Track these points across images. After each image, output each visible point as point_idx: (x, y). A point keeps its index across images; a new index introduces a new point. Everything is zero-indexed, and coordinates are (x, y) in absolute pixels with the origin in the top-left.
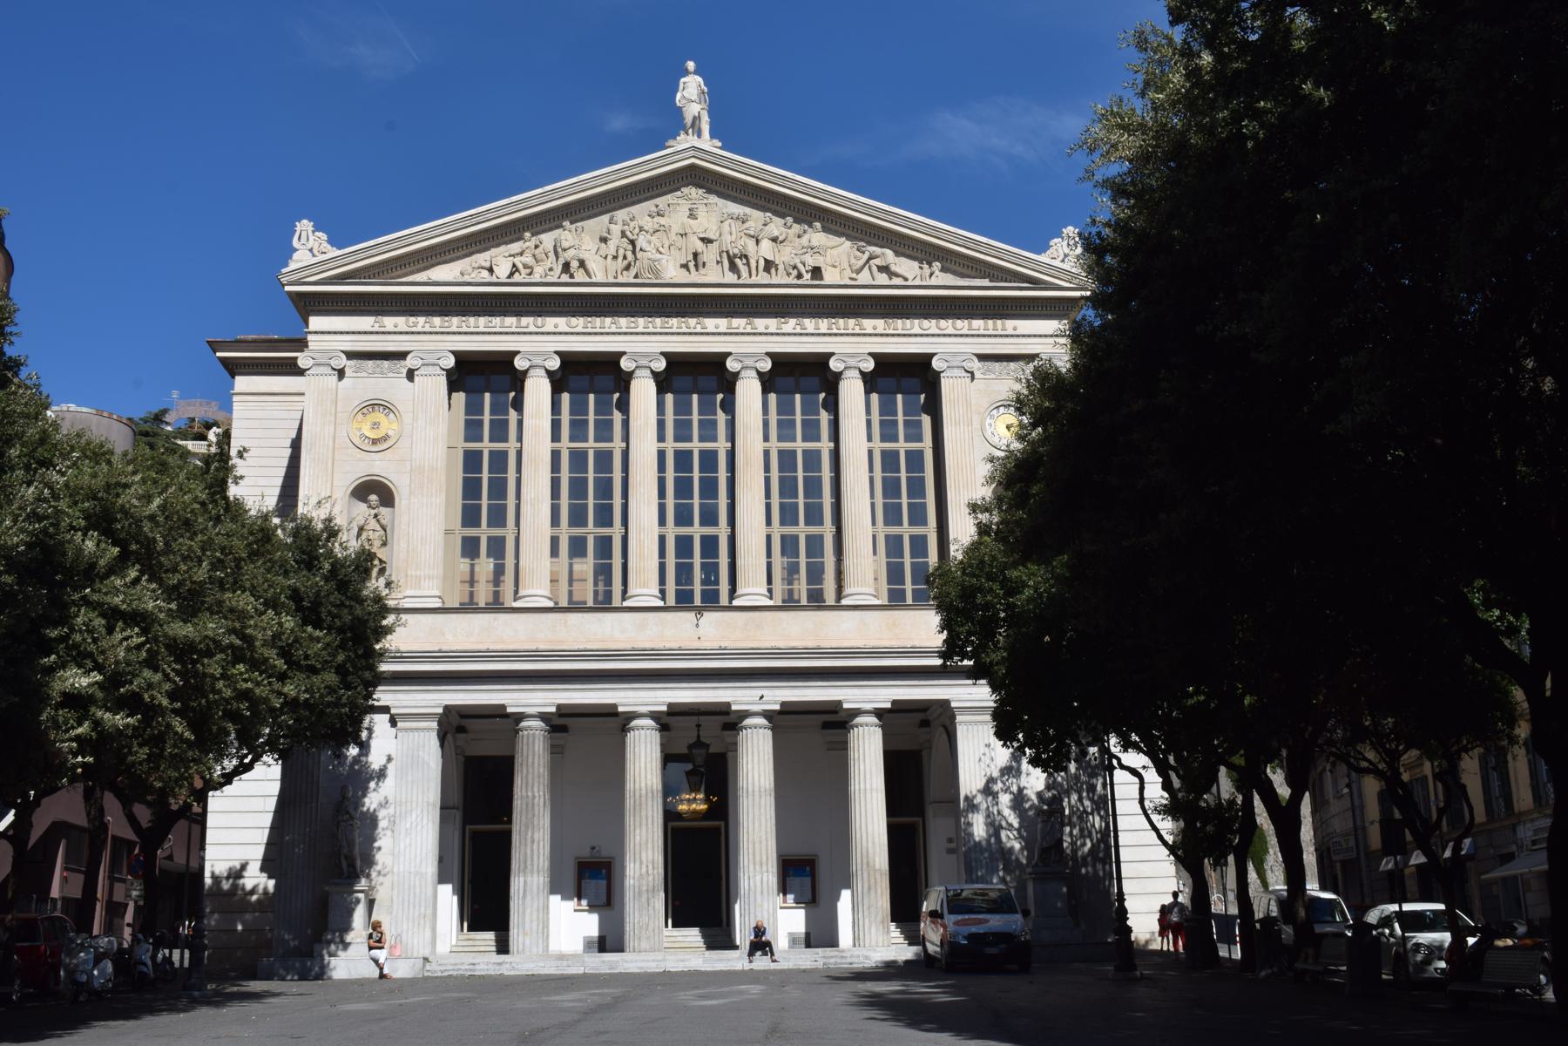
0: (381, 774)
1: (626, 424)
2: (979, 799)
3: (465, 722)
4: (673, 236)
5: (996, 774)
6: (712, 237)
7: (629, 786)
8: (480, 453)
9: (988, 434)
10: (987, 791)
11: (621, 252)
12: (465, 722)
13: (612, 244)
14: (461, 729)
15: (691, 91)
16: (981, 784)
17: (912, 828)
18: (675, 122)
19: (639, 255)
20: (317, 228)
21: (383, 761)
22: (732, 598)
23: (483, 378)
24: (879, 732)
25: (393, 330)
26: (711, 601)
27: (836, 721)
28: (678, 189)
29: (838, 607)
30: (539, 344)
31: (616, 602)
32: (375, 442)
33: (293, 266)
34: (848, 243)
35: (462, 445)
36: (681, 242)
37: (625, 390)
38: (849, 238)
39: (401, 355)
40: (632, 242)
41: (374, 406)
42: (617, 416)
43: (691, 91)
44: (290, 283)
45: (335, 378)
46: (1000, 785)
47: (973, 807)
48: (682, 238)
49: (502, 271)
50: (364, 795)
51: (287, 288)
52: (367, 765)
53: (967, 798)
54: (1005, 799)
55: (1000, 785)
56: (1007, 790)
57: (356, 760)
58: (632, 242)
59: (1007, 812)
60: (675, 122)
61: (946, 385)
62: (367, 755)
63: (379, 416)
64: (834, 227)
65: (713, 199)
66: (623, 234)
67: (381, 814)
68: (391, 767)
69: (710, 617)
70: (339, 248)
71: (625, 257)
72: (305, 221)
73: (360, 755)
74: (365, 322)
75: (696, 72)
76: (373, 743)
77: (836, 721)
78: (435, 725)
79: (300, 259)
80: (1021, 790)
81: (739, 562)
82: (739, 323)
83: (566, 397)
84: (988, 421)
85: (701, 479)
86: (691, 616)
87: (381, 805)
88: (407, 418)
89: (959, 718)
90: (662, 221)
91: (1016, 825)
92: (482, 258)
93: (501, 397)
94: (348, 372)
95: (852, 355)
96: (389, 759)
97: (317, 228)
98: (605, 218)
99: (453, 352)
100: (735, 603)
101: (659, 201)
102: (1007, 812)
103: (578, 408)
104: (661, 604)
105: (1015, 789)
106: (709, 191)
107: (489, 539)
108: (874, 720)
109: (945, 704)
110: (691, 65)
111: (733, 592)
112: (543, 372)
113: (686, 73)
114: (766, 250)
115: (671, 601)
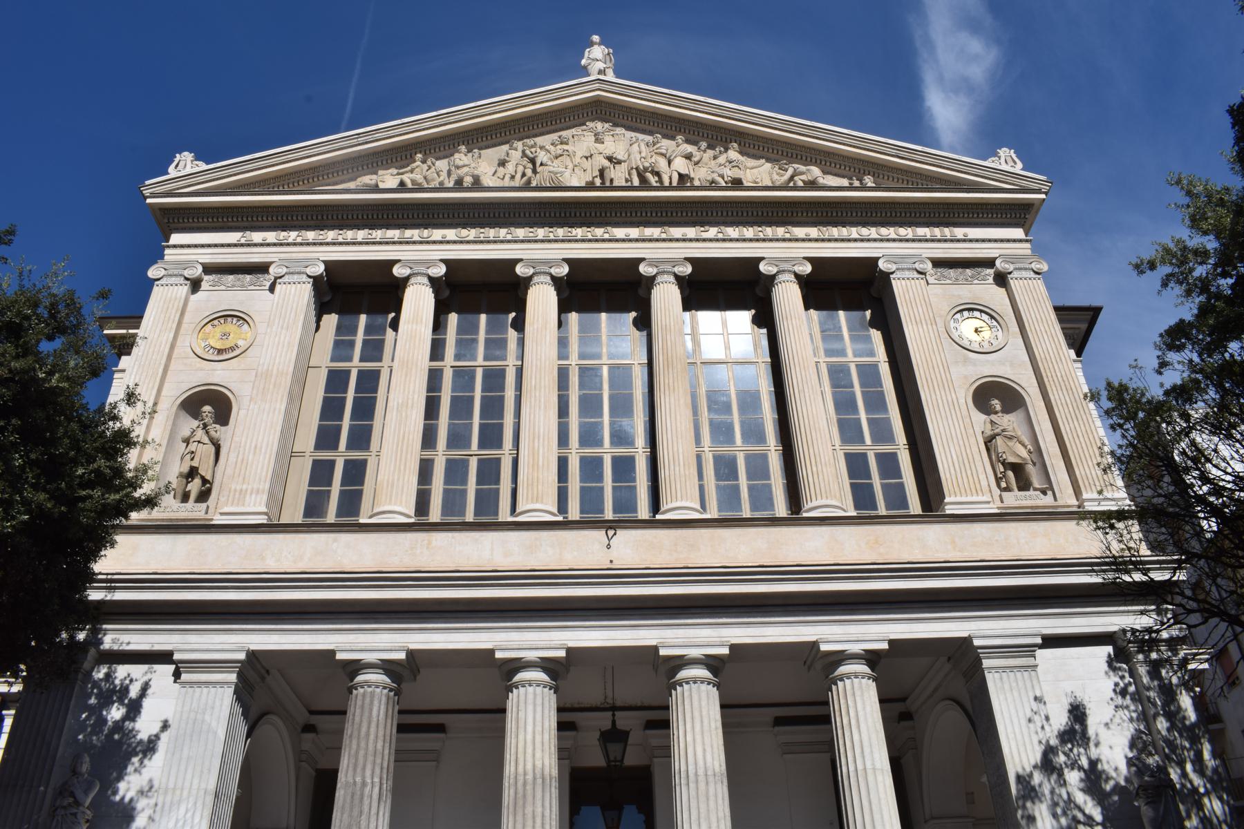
0: (149, 747)
1: (521, 342)
2: (1037, 778)
3: (315, 720)
4: (577, 160)
5: (1054, 742)
6: (620, 157)
7: (509, 769)
8: (347, 373)
9: (955, 335)
10: (1047, 764)
11: (520, 168)
12: (315, 720)
13: (510, 168)
14: (309, 728)
16: (1036, 756)
19: (539, 169)
21: (155, 729)
22: (655, 506)
23: (359, 295)
24: (872, 686)
25: (260, 245)
28: (584, 124)
30: (421, 255)
31: (504, 515)
32: (220, 351)
34: (768, 165)
36: (587, 164)
37: (520, 306)
38: (768, 160)
40: (533, 161)
41: (227, 316)
42: (512, 335)
44: (154, 195)
45: (185, 289)
46: (1062, 758)
47: (1029, 792)
50: (120, 778)
51: (149, 201)
52: (132, 733)
53: (1019, 778)
54: (1073, 777)
55: (1062, 758)
56: (1074, 765)
57: (118, 726)
58: (533, 161)
59: (1080, 798)
61: (898, 286)
62: (133, 720)
63: (231, 326)
64: (751, 151)
65: (620, 130)
66: (524, 154)
67: (141, 804)
68: (164, 737)
69: (624, 537)
70: (207, 163)
71: (524, 175)
72: (186, 153)
73: (124, 719)
75: (600, 44)
76: (147, 703)
78: (233, 677)
80: (1093, 763)
81: (663, 474)
83: (453, 318)
84: (952, 324)
85: (601, 415)
86: (599, 535)
87: (141, 792)
88: (261, 328)
89: (986, 663)
90: (565, 147)
91: (1098, 818)
93: (379, 319)
94: (204, 285)
95: (786, 260)
96: (165, 726)
98: (505, 147)
99: (324, 262)
100: (658, 517)
101: (564, 133)
102: (1080, 798)
103: (467, 330)
104: (560, 518)
105: (1084, 762)
106: (616, 125)
107: (347, 462)
108: (863, 668)
109: (966, 642)
110: (596, 38)
111: (655, 506)
112: (425, 280)
113: (592, 44)
114: (680, 165)
115: (574, 513)
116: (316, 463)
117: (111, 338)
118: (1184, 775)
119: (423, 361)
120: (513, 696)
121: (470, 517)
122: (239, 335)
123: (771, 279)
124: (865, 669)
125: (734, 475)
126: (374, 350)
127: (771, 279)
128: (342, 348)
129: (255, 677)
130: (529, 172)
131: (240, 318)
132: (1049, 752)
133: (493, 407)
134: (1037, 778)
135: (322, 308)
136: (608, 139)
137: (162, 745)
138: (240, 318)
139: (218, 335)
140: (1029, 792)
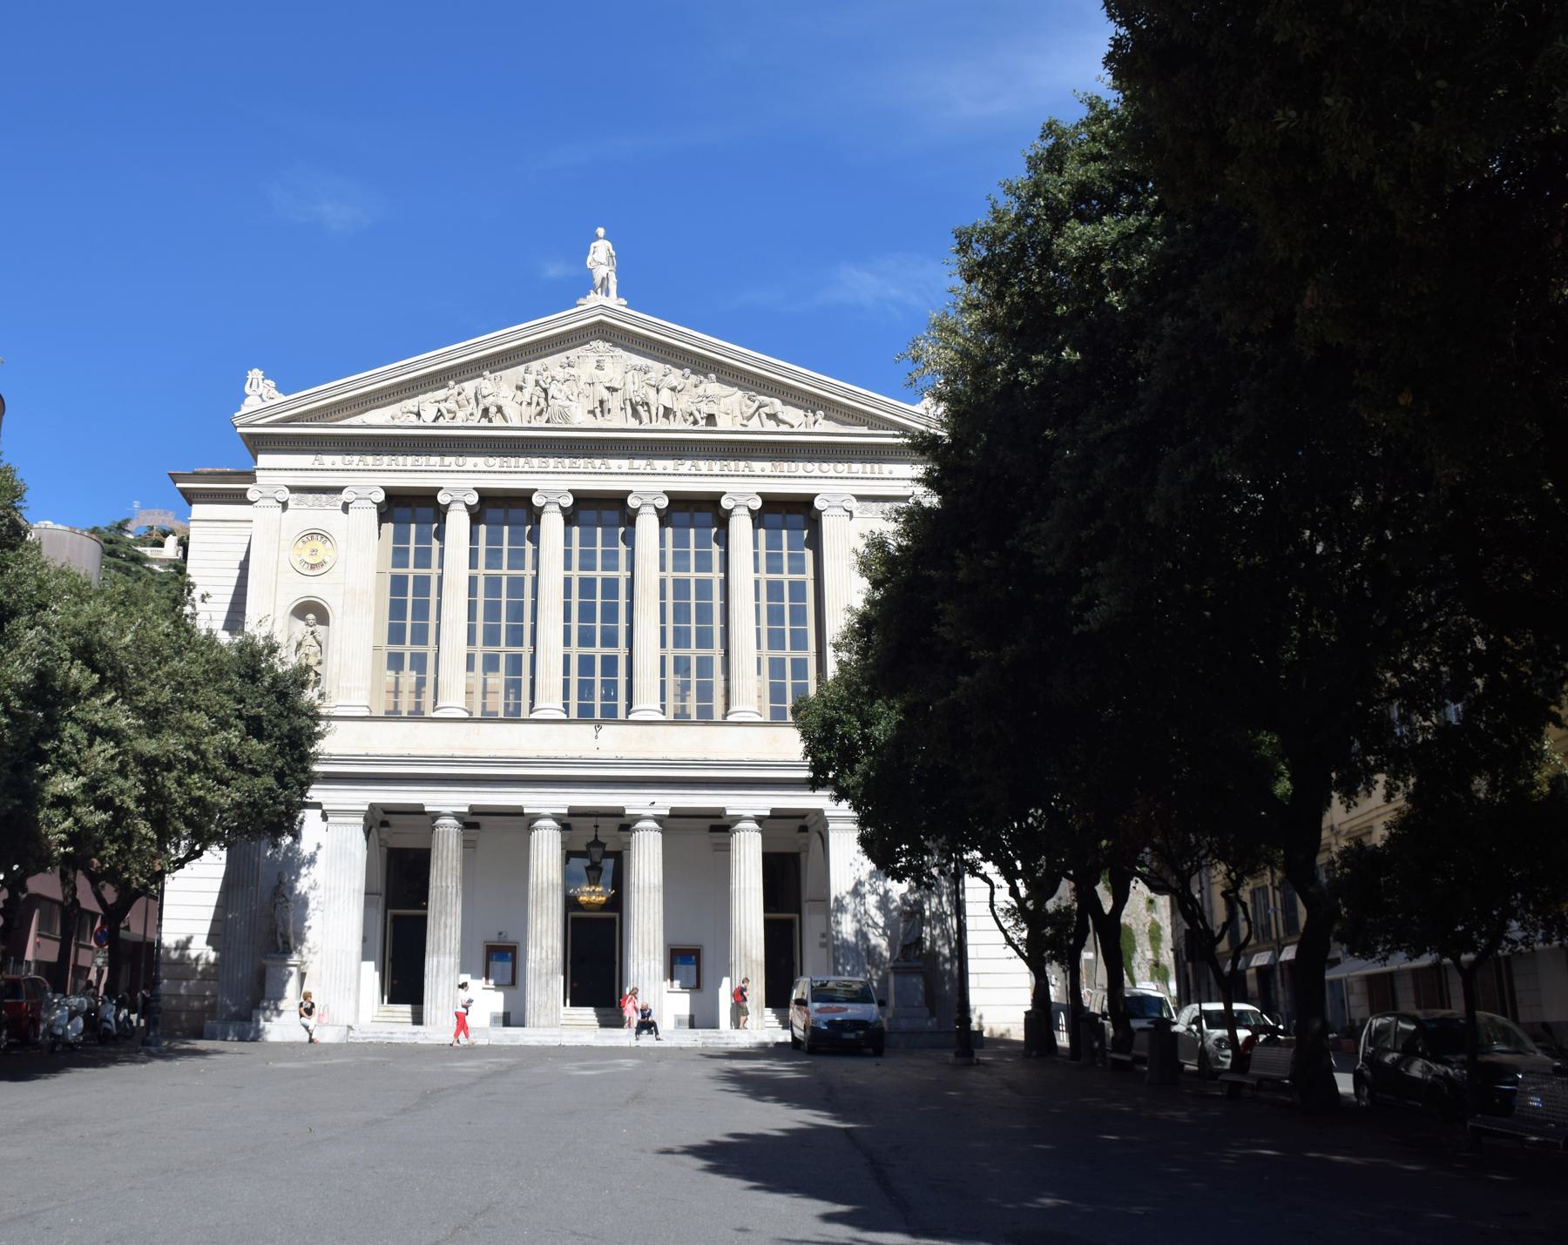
0: (312, 860)
1: (536, 553)
2: (848, 899)
4: (581, 385)
10: (856, 892)
11: (535, 399)
15: (600, 256)
16: (850, 886)
17: (789, 924)
18: (585, 284)
19: (551, 402)
20: (266, 376)
21: (313, 849)
22: (628, 713)
23: (409, 509)
24: (759, 836)
26: (610, 715)
27: (720, 826)
29: (627, 722)
31: (525, 714)
32: (313, 567)
33: (245, 410)
34: (740, 393)
35: (390, 570)
36: (588, 390)
38: (741, 388)
39: (338, 490)
40: (545, 391)
41: (313, 534)
43: (600, 256)
46: (867, 887)
47: (841, 908)
48: (589, 387)
49: (428, 416)
52: (298, 852)
53: (836, 899)
54: (872, 900)
56: (874, 892)
58: (545, 391)
59: (874, 912)
60: (585, 284)
63: (317, 543)
67: (311, 896)
69: (608, 730)
74: (306, 460)
77: (720, 826)
78: (361, 820)
79: (251, 404)
82: (640, 464)
86: (591, 728)
92: (411, 404)
95: (742, 495)
96: (319, 847)
97: (266, 376)
99: (383, 488)
104: (564, 717)
105: (881, 891)
110: (601, 231)
113: (597, 238)
114: (666, 398)
115: (574, 714)
116: (390, 655)
117: (183, 491)
118: (940, 903)
119: (465, 572)
120: (535, 834)
121: (501, 715)
122: (324, 552)
123: (729, 513)
124: (756, 826)
125: (687, 671)
126: (423, 559)
127: (729, 513)
128: (399, 557)
129: (378, 821)
130: (542, 401)
131: (323, 536)
132: (859, 883)
133: (516, 612)
134: (848, 899)
135: (383, 518)
136: (608, 363)
137: (320, 857)
138: (323, 536)
139: (308, 551)
140: (841, 908)
